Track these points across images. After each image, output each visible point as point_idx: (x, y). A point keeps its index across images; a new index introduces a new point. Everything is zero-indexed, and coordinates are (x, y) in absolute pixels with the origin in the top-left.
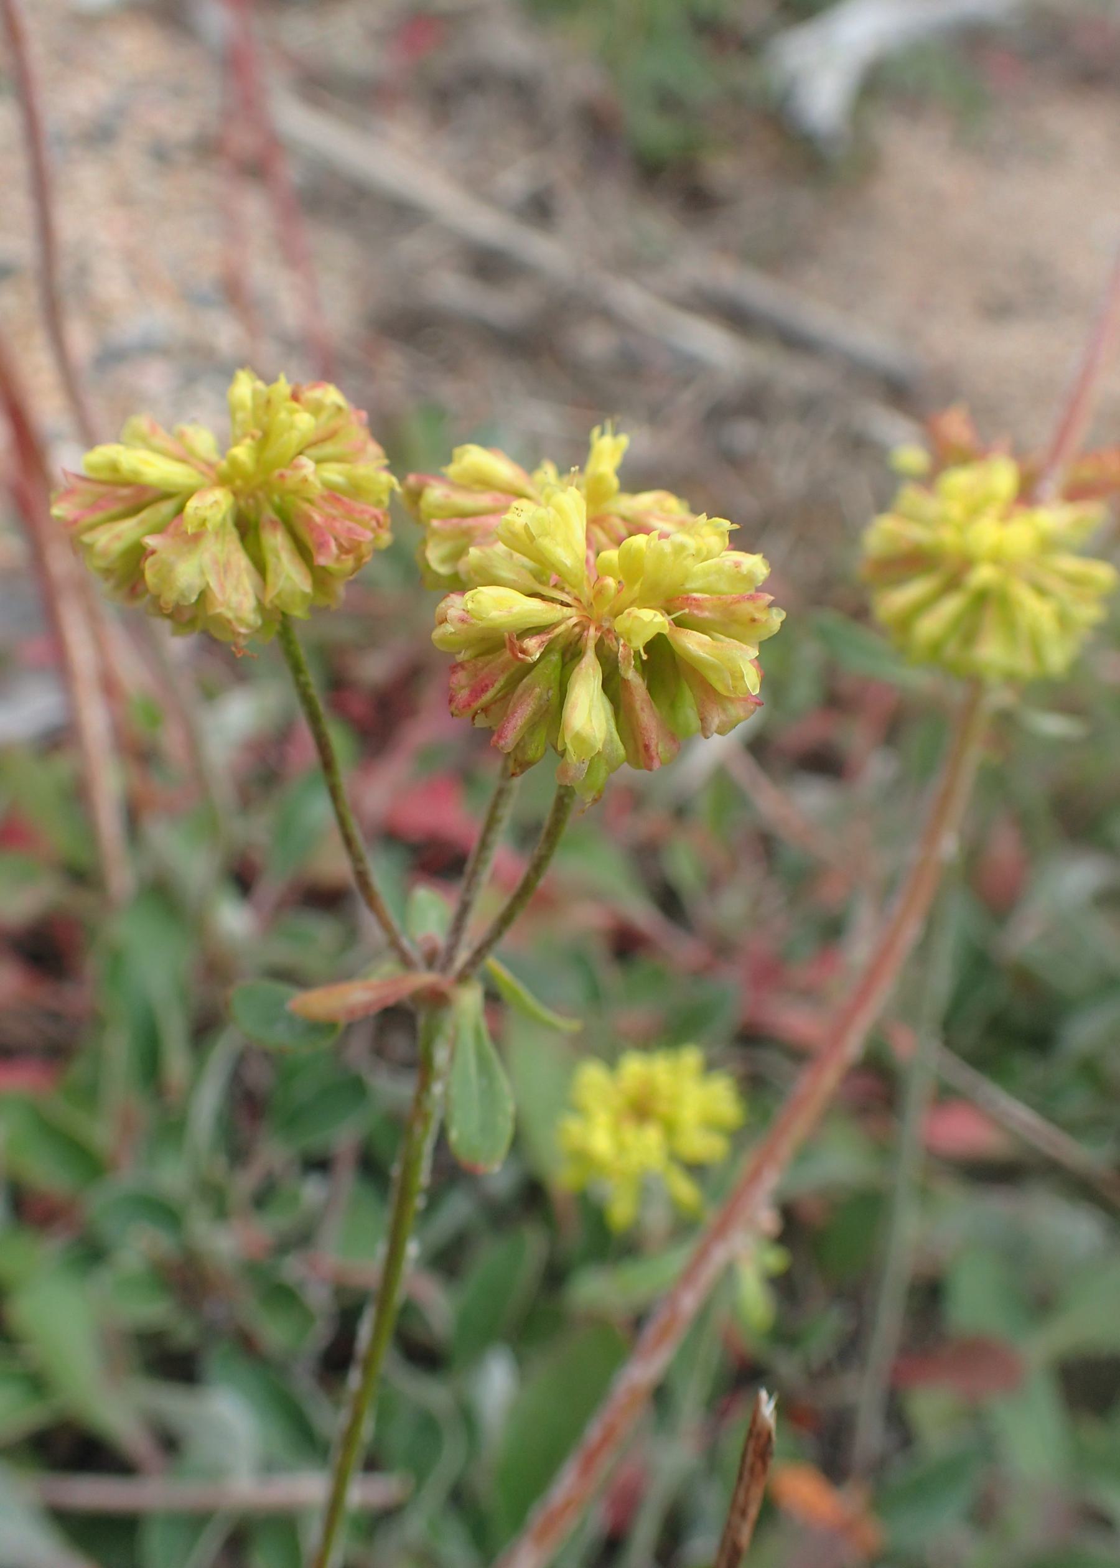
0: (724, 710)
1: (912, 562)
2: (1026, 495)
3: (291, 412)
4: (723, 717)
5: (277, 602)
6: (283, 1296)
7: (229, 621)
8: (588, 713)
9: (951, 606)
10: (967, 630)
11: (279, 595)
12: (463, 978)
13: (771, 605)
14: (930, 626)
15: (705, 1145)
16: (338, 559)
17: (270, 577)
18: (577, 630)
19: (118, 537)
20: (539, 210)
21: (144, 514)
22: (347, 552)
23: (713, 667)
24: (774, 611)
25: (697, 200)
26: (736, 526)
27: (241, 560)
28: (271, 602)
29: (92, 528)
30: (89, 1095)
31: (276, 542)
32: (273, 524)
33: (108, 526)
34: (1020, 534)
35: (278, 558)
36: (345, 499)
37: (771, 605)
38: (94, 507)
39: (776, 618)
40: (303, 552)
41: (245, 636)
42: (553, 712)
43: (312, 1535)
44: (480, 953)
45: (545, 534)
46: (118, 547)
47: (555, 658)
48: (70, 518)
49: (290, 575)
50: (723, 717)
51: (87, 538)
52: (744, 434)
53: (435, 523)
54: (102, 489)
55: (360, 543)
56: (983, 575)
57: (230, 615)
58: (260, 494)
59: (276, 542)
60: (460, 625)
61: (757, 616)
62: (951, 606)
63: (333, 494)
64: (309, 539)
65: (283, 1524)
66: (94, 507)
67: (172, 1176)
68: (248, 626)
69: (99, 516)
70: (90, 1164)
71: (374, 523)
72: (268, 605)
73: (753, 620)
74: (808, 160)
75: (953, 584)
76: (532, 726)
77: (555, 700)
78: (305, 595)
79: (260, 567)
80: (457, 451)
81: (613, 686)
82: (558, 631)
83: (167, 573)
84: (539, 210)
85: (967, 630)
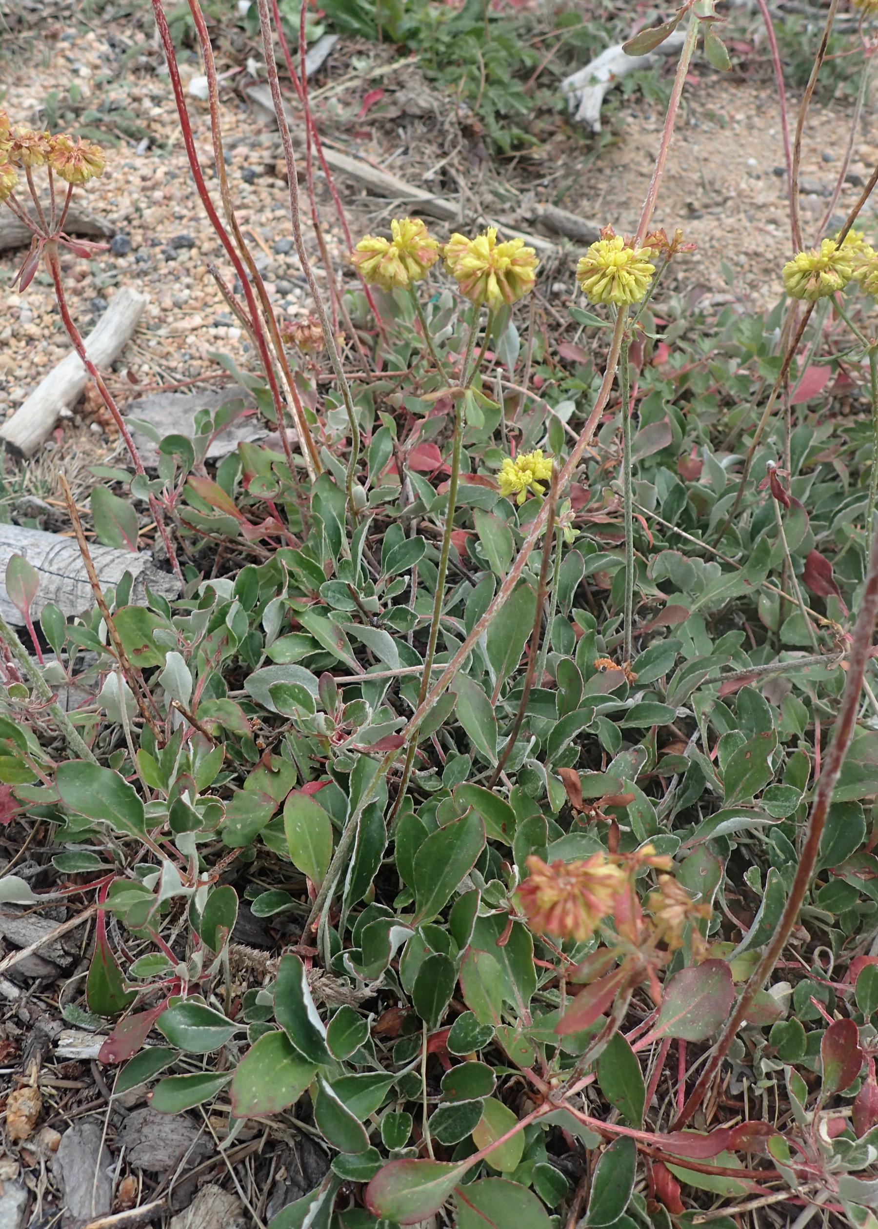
1: (592, 271)
8: (493, 286)
9: (604, 281)
10: (608, 288)
12: (467, 387)
14: (597, 289)
20: (446, 183)
25: (528, 171)
27: (402, 266)
30: (315, 552)
31: (410, 261)
34: (622, 257)
40: (417, 263)
42: (485, 290)
49: (415, 269)
56: (611, 269)
59: (410, 261)
62: (604, 281)
63: (423, 248)
74: (585, 140)
75: (604, 275)
79: (407, 268)
81: (499, 282)
83: (386, 269)
84: (446, 183)
85: (608, 288)
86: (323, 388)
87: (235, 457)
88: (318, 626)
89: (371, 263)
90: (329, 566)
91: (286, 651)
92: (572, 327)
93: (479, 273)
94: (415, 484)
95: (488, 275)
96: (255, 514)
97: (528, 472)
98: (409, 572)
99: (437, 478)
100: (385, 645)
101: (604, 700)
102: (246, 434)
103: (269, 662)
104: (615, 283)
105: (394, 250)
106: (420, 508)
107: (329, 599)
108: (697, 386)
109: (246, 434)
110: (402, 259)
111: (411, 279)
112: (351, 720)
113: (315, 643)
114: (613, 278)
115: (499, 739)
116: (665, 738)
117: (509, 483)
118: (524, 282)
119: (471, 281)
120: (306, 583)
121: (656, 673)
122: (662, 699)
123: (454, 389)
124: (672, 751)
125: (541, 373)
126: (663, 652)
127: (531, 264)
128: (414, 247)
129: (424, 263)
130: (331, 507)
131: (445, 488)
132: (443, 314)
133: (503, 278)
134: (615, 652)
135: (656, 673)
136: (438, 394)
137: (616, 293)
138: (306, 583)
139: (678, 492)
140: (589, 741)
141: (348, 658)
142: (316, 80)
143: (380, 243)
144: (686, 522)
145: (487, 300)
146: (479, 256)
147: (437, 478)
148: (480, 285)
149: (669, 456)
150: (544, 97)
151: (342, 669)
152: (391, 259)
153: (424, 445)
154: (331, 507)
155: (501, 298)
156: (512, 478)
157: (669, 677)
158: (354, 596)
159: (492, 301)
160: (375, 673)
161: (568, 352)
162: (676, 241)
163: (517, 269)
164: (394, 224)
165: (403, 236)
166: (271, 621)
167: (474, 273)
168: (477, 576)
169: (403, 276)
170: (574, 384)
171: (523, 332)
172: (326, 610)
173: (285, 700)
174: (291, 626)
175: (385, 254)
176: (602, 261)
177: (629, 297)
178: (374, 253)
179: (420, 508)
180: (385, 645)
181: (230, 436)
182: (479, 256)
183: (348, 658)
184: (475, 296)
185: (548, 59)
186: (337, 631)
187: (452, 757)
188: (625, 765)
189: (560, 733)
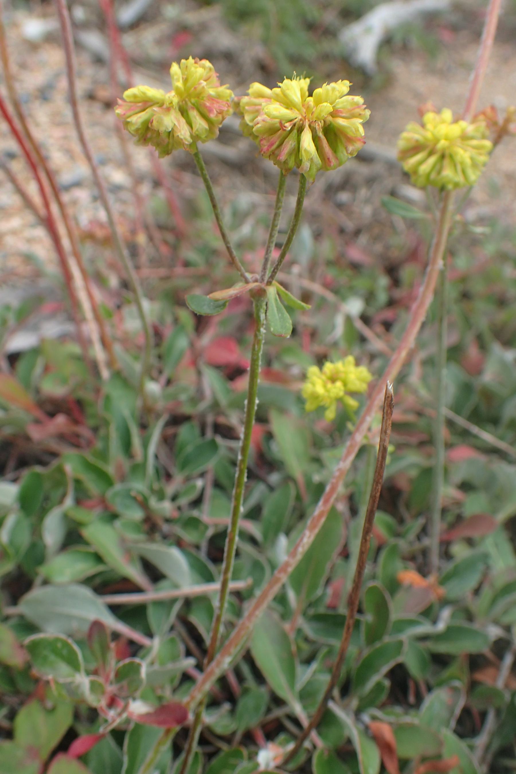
0: (353, 145)
1: (416, 148)
2: (456, 121)
3: (196, 68)
4: (353, 147)
5: (197, 133)
6: (193, 523)
7: (182, 139)
8: (307, 141)
9: (432, 160)
10: (438, 168)
11: (197, 130)
12: (269, 283)
13: (365, 109)
14: (424, 168)
15: (362, 387)
16: (217, 116)
17: (193, 126)
18: (301, 122)
19: (140, 117)
21: (147, 110)
22: (220, 113)
23: (349, 127)
24: (367, 110)
26: (351, 84)
27: (183, 121)
28: (195, 133)
29: (130, 116)
30: (104, 455)
31: (194, 114)
32: (193, 108)
33: (135, 115)
35: (196, 119)
36: (216, 99)
37: (365, 109)
38: (130, 110)
39: (368, 113)
40: (204, 116)
41: (187, 145)
42: (297, 150)
43: (216, 603)
44: (274, 273)
45: (288, 89)
46: (140, 121)
47: (295, 131)
48: (123, 113)
49: (200, 124)
50: (353, 147)
51: (129, 120)
52: (344, 197)
53: (247, 108)
54: (132, 104)
55: (223, 111)
57: (182, 137)
58: (187, 99)
59: (194, 114)
60: (263, 123)
61: (361, 113)
62: (432, 160)
63: (211, 98)
64: (205, 111)
65: (203, 600)
66: (130, 110)
67: (139, 486)
68: (188, 141)
69: (132, 112)
70: (105, 479)
71: (227, 105)
72: (194, 135)
73: (360, 114)
75: (431, 153)
76: (290, 154)
77: (297, 146)
78: (206, 129)
79: (190, 124)
80: (251, 85)
81: (315, 139)
82: (296, 120)
83: (160, 122)
85: (438, 168)
86: (125, 285)
87: (36, 351)
88: (102, 536)
89: (143, 116)
90: (119, 468)
91: (65, 569)
92: (357, 233)
93: (288, 126)
94: (212, 381)
95: (300, 130)
96: (51, 408)
97: (339, 384)
98: (202, 475)
99: (233, 373)
100: (175, 561)
101: (412, 623)
102: (52, 329)
103: (46, 582)
104: (446, 162)
105: (172, 97)
106: (215, 405)
107: (118, 506)
108: (478, 287)
109: (52, 329)
110: (183, 112)
111: (195, 138)
112: (125, 683)
113: (98, 558)
114: (443, 157)
115: (299, 669)
116: (476, 662)
117: (315, 397)
118: (350, 140)
119: (276, 139)
120: (93, 486)
121: (462, 588)
122: (470, 617)
123: (253, 285)
124: (484, 677)
125: (331, 273)
126: (469, 565)
127: (360, 116)
128: (198, 95)
129: (212, 116)
130: (123, 406)
131: (243, 384)
132: (239, 217)
133: (321, 134)
134: (421, 562)
135: (462, 588)
136: (232, 292)
137: (448, 173)
138: (93, 486)
139: (466, 389)
140: (399, 677)
141: (135, 573)
142: (136, 25)
143: (153, 92)
144: (476, 417)
145: (299, 163)
146: (288, 104)
147: (233, 373)
148: (290, 144)
149: (455, 353)
150: (326, 46)
151: (126, 586)
152: (168, 109)
153: (220, 342)
154: (123, 406)
155: (318, 160)
156: (320, 390)
157: (477, 591)
158: (144, 504)
159: (306, 164)
160: (162, 592)
161: (355, 254)
162: (508, 121)
163: (341, 122)
164: (175, 68)
165: (185, 81)
166: (52, 532)
167: (282, 126)
168: (274, 478)
169: (184, 133)
170: (362, 283)
171: (317, 236)
172: (113, 517)
173: (45, 658)
174: (73, 538)
175: (160, 104)
176: (429, 135)
177: (459, 178)
178: (146, 103)
179: (215, 405)
180: (175, 561)
181: (36, 328)
182: (288, 104)
183: (135, 573)
184: (283, 157)
185: (329, 17)
186: (123, 541)
187: (246, 691)
188: (440, 703)
189: (367, 667)
